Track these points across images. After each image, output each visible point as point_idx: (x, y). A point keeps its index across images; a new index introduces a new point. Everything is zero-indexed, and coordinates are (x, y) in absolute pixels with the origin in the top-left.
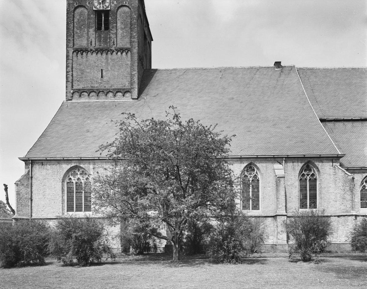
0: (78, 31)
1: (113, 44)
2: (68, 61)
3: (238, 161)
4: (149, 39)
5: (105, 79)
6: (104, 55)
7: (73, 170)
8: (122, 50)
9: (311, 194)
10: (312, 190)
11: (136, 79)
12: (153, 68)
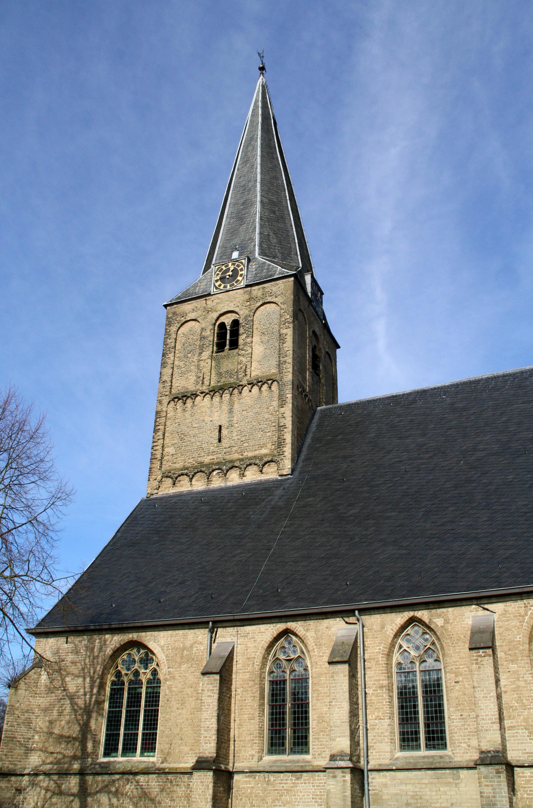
0: (181, 364)
1: (243, 374)
2: (158, 419)
3: (216, 632)
4: (324, 346)
5: (225, 442)
6: (226, 396)
7: (127, 652)
8: (259, 382)
9: (442, 739)
10: (407, 720)
11: (288, 437)
12: (353, 399)
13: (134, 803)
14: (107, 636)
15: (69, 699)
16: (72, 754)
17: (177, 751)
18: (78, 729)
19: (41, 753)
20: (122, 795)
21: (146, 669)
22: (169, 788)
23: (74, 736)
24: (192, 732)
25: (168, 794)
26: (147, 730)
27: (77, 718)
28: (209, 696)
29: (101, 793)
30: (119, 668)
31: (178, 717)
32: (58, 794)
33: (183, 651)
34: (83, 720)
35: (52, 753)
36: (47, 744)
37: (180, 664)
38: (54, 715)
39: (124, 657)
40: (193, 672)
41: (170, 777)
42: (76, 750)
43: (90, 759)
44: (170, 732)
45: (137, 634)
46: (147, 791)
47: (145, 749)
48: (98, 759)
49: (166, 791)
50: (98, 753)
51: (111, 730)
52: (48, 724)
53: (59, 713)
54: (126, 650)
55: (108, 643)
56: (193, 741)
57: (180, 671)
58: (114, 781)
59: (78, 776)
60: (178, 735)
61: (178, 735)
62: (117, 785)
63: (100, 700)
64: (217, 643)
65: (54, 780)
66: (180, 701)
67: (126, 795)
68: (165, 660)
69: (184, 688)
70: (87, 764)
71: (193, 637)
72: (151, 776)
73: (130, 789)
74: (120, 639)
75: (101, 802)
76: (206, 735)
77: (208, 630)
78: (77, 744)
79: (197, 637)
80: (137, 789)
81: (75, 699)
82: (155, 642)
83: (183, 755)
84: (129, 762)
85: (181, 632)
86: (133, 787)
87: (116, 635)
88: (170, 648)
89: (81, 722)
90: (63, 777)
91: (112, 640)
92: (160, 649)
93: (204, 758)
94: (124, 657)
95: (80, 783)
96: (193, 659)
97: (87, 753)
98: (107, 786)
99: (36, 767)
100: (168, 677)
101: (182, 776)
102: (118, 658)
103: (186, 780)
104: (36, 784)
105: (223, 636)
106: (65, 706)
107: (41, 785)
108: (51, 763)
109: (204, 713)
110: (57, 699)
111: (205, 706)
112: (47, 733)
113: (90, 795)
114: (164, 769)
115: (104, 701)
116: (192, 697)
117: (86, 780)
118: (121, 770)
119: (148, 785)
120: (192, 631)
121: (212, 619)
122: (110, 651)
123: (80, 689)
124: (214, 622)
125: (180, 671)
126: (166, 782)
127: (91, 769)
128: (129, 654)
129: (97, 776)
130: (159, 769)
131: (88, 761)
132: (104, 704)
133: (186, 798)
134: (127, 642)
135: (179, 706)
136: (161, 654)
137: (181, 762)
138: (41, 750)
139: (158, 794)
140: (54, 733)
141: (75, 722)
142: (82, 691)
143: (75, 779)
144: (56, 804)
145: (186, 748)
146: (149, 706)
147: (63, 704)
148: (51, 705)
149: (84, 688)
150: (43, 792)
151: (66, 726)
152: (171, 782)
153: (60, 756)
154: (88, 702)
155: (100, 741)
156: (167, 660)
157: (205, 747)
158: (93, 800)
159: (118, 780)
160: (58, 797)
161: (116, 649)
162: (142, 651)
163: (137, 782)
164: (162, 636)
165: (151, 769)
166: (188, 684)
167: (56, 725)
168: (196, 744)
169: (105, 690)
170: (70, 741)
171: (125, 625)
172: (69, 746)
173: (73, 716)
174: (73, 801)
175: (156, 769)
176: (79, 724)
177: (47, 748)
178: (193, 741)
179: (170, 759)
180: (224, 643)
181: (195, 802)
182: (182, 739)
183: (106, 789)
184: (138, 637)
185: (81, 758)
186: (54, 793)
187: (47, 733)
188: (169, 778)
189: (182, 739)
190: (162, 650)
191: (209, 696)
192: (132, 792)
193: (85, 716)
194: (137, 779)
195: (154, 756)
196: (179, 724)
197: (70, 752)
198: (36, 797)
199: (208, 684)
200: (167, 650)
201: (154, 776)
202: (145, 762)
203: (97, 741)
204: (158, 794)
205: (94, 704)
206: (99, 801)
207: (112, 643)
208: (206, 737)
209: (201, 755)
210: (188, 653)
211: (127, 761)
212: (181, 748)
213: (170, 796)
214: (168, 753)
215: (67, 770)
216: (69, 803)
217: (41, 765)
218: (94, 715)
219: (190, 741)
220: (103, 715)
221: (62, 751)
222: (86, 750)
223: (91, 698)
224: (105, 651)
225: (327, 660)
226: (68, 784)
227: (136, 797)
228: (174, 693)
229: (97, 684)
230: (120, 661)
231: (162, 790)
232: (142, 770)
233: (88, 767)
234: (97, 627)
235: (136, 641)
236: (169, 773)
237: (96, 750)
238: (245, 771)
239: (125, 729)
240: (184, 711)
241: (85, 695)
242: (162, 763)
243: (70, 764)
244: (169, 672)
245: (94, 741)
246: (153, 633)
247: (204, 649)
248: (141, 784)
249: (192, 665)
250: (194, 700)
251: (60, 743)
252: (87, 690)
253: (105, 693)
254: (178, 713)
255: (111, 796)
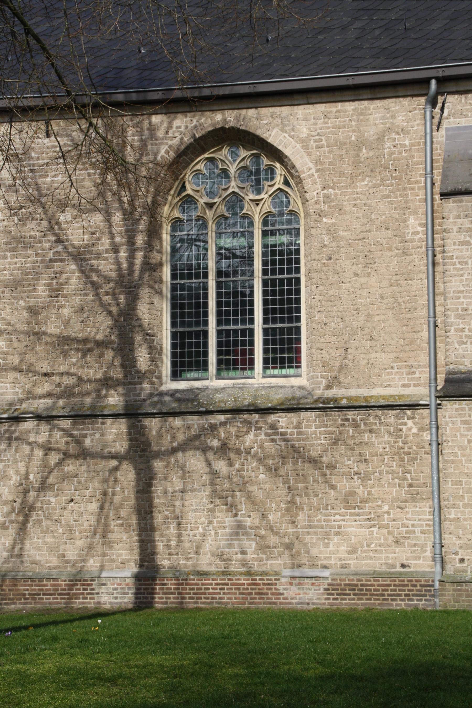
7: (206, 155)
13: (270, 469)
14: (156, 119)
15: (75, 259)
16: (99, 375)
17: (364, 362)
18: (109, 322)
19: (18, 375)
20: (238, 452)
21: (259, 192)
22: (353, 437)
23: (99, 337)
24: (396, 324)
25: (352, 449)
26: (274, 321)
27: (100, 300)
28: (463, 243)
29: (184, 451)
30: (189, 191)
31: (359, 292)
32: (76, 457)
33: (360, 149)
34: (118, 305)
35: (46, 375)
36: (30, 358)
37: (353, 179)
38: (39, 297)
39: (197, 167)
40: (388, 197)
41: (351, 415)
42: (109, 368)
43: (146, 385)
44: (341, 325)
45: (236, 112)
46: (297, 444)
47: (274, 361)
48: (161, 384)
49: (345, 444)
50: (160, 373)
51: (183, 324)
52: (26, 315)
53: (50, 290)
54: (204, 152)
55: (160, 133)
56: (402, 342)
57: (353, 193)
58: (213, 427)
59: (124, 420)
60: (362, 329)
61: (362, 329)
62: (223, 435)
63: (154, 261)
64: (447, 129)
65: (63, 430)
66: (361, 260)
67: (248, 453)
68: (313, 171)
69: (369, 231)
70: (139, 394)
71: (383, 118)
72: (303, 415)
73: (256, 441)
74: (190, 126)
75: (188, 468)
76: (461, 326)
77: (423, 100)
78: (109, 354)
79: (393, 117)
80: (273, 440)
81: (90, 259)
82: (282, 130)
83: (377, 370)
84: (241, 388)
85: (350, 107)
86: (263, 437)
87: (180, 116)
88: (324, 142)
89: (114, 309)
90: (84, 423)
91: (170, 127)
92: (299, 146)
93: (461, 373)
94: (197, 167)
95: (129, 433)
96: (386, 168)
97: (138, 372)
98: (197, 437)
99: (11, 404)
100: (325, 207)
101: (380, 412)
102: (185, 168)
103: (392, 420)
104: (17, 439)
105: (462, 114)
106: (64, 276)
107: (31, 439)
108: (49, 395)
109: (453, 279)
110: (42, 261)
111: (454, 264)
112: (27, 334)
113: (158, 455)
114: (336, 400)
115: (161, 264)
116: (390, 249)
117: (143, 427)
118: (229, 405)
119: (299, 433)
120: (379, 103)
121: (440, 73)
122: (167, 152)
123: (99, 239)
124: (441, 81)
125: (353, 193)
126: (342, 425)
127: (154, 404)
128: (212, 160)
129: (171, 419)
130: (326, 401)
131: (142, 389)
132: (161, 270)
133: (396, 457)
134: (210, 132)
135: (358, 269)
136: (302, 157)
137: (374, 386)
138: (18, 369)
139: (326, 451)
140: (45, 333)
141: (97, 308)
142: (105, 243)
143: (116, 425)
144: (76, 475)
145: (383, 355)
146: (274, 272)
147: (61, 273)
148: (27, 274)
149: (112, 236)
150: (39, 453)
151: (74, 319)
152: (356, 425)
153: (68, 381)
154: (125, 266)
155: (161, 347)
156: (318, 170)
157: (461, 351)
158: (167, 466)
159: (223, 424)
160: (78, 462)
161: (183, 147)
162: (243, 153)
163: (273, 427)
164: (300, 116)
165: (302, 401)
166: (378, 222)
167: (47, 318)
168: (408, 348)
169: (160, 239)
170: (90, 350)
171: (206, 92)
172: (89, 359)
173: (91, 297)
174: (116, 469)
175: (316, 401)
176: (110, 313)
177: (31, 365)
178: (402, 342)
179: (346, 380)
180: (465, 128)
181: (453, 462)
182: (372, 338)
183: (197, 443)
184: (237, 119)
185: (124, 384)
186: (66, 455)
187: (27, 334)
188: (349, 417)
189: (372, 338)
190: (305, 147)
191: (463, 243)
192: (261, 447)
193: (122, 297)
194: (269, 421)
195: (300, 376)
196: (362, 308)
197: (92, 371)
198: (21, 466)
199: (459, 217)
200: (318, 147)
201: (312, 415)
202: (281, 387)
203: (155, 348)
204: (326, 451)
205: (142, 271)
206: (183, 468)
207: (170, 135)
208: (463, 330)
209: (452, 367)
210: (371, 154)
211: (234, 387)
212: (373, 356)
213: (357, 452)
214: (341, 369)
215: (93, 407)
216: (107, 474)
217: (21, 401)
218: (145, 293)
219: (393, 342)
220: (161, 293)
221: (73, 370)
222: (135, 366)
223: (131, 258)
224: (156, 154)
225: (439, 192)
226: (97, 435)
227: (273, 457)
228: (343, 243)
229: (142, 226)
230: (188, 176)
231: (335, 442)
232: (282, 404)
233: (144, 400)
234: (134, 97)
235: (233, 129)
236: (349, 408)
237: (157, 366)
238: (421, 402)
239: (219, 323)
240: (373, 280)
241: (115, 249)
242: (329, 387)
243: (99, 396)
244: (325, 196)
245: (150, 347)
246: (277, 109)
247: (411, 145)
248: (280, 430)
249: (382, 180)
250: (397, 255)
251: (65, 354)
252: (118, 239)
253: (161, 247)
254: (358, 285)
255: (211, 456)
